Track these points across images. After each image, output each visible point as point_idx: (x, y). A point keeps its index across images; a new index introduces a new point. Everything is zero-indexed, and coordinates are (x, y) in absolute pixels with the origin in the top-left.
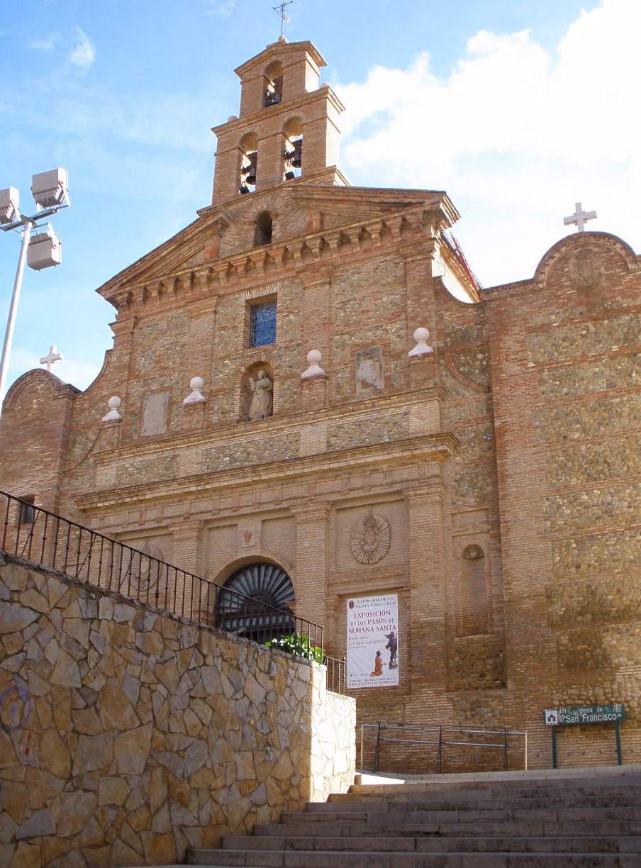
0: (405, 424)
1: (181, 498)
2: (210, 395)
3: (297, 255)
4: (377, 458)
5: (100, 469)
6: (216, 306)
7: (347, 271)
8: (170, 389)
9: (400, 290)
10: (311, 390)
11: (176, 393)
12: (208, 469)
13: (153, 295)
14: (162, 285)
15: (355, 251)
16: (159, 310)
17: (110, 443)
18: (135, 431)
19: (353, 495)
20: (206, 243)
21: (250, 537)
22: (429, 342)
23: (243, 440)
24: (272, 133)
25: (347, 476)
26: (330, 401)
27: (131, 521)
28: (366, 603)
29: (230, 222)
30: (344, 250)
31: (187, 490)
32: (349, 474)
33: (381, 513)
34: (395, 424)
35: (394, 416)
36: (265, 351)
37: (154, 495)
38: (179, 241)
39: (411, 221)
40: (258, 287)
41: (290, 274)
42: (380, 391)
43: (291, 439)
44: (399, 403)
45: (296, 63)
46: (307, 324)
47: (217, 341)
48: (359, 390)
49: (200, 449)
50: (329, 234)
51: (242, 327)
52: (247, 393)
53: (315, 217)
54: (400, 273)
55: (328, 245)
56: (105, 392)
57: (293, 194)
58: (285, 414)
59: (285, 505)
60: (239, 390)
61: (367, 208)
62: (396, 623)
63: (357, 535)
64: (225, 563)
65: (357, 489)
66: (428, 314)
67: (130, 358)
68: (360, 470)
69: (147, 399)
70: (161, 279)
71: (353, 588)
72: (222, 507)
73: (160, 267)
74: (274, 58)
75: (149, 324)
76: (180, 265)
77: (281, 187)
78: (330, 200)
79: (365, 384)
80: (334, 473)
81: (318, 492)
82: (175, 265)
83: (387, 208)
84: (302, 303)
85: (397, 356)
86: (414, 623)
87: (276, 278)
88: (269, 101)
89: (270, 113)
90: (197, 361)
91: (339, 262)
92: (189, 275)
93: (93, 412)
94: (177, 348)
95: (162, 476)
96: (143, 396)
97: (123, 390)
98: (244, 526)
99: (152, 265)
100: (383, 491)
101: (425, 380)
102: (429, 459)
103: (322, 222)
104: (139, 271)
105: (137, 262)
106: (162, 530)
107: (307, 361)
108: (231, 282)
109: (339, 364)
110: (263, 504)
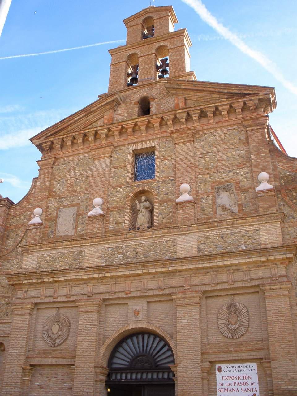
0: (258, 237)
1: (86, 282)
2: (107, 210)
3: (170, 123)
4: (241, 261)
5: (26, 256)
6: (111, 153)
7: (205, 134)
8: (78, 205)
9: (244, 147)
10: (183, 210)
11: (82, 208)
12: (106, 262)
13: (68, 144)
14: (74, 138)
15: (210, 122)
16: (71, 154)
17: (34, 239)
18: (52, 232)
19: (219, 287)
20: (105, 114)
21: (138, 314)
22: (269, 182)
23: (133, 243)
24: (148, 54)
25: (215, 273)
26: (198, 219)
27: (47, 295)
28: (231, 369)
29: (121, 102)
30: (202, 121)
31: (91, 276)
32: (217, 271)
33: (241, 301)
34: (249, 237)
35: (248, 231)
36: (147, 183)
37: (66, 278)
38: (87, 111)
39: (250, 105)
40: (142, 142)
41: (165, 135)
42: (235, 214)
43: (170, 244)
44: (252, 222)
45: (162, 17)
46: (179, 167)
47: (112, 175)
48: (219, 211)
49: (100, 248)
50: (193, 110)
51: (130, 167)
52: (135, 212)
53: (181, 101)
54: (243, 137)
55: (192, 118)
56: (31, 205)
57: (167, 85)
58: (161, 227)
59: (166, 292)
60: (129, 208)
61: (218, 96)
62: (257, 386)
63: (223, 317)
64: (118, 331)
65: (224, 283)
66: (266, 163)
67: (50, 184)
68: (226, 269)
69: (61, 211)
70: (74, 134)
71: (222, 357)
72: (117, 290)
73: (73, 127)
74: (148, 15)
75: (64, 163)
76: (86, 127)
77: (156, 83)
78: (193, 90)
79: (224, 208)
80: (205, 271)
81: (192, 283)
82: (83, 126)
83: (231, 95)
84: (173, 154)
85: (246, 190)
86: (277, 390)
87: (155, 137)
88: (145, 37)
89: (146, 42)
90: (98, 188)
91: (200, 128)
92: (94, 132)
93: (22, 217)
94: (84, 179)
95: (71, 264)
96: (58, 209)
97: (44, 204)
98: (133, 305)
99: (68, 125)
100: (243, 285)
101: (270, 207)
102: (278, 263)
103: (185, 104)
104: (59, 129)
105: (58, 123)
106: (73, 304)
107: (179, 191)
108: (122, 138)
109: (203, 194)
110: (149, 290)
